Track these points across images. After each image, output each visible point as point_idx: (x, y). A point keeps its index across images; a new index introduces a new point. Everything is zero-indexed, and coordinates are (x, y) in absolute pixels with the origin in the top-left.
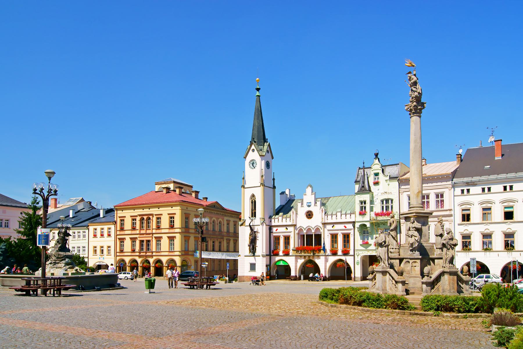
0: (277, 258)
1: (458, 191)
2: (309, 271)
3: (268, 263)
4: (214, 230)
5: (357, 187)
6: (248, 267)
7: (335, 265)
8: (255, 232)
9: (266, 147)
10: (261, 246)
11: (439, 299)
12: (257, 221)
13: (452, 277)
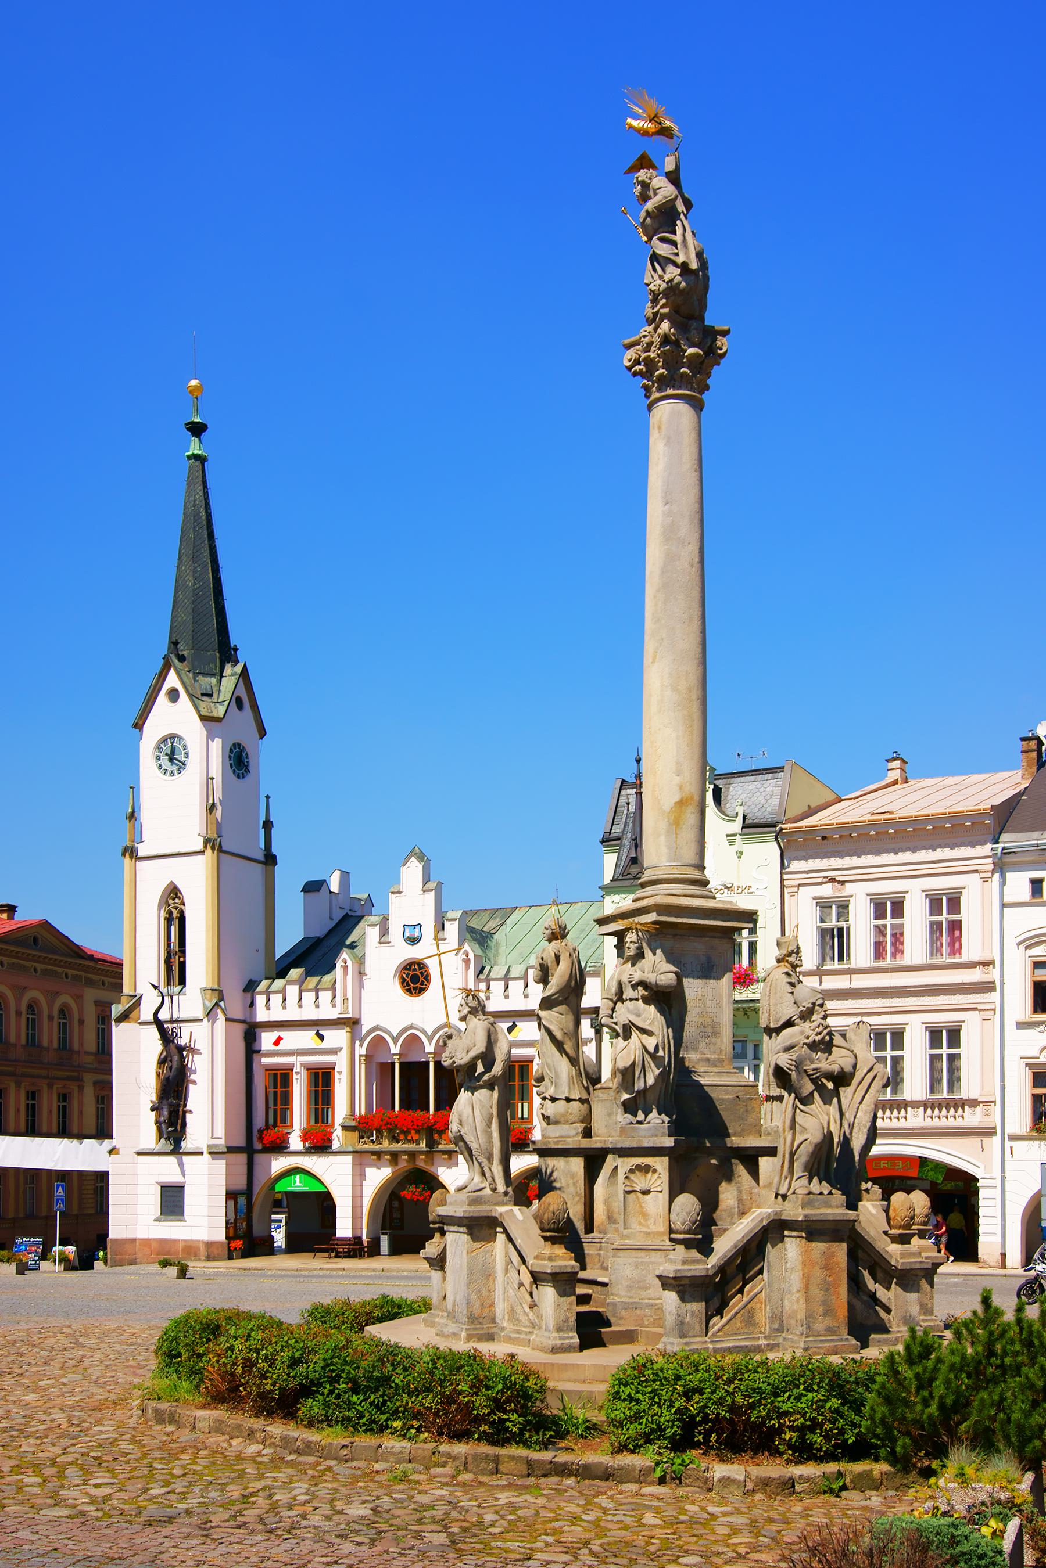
0: (279, 1164)
1: (1018, 883)
3: (241, 1183)
4: (33, 1041)
5: (610, 862)
6: (153, 1201)
8: (181, 1049)
9: (228, 683)
11: (695, 1380)
12: (191, 1002)
13: (819, 1247)
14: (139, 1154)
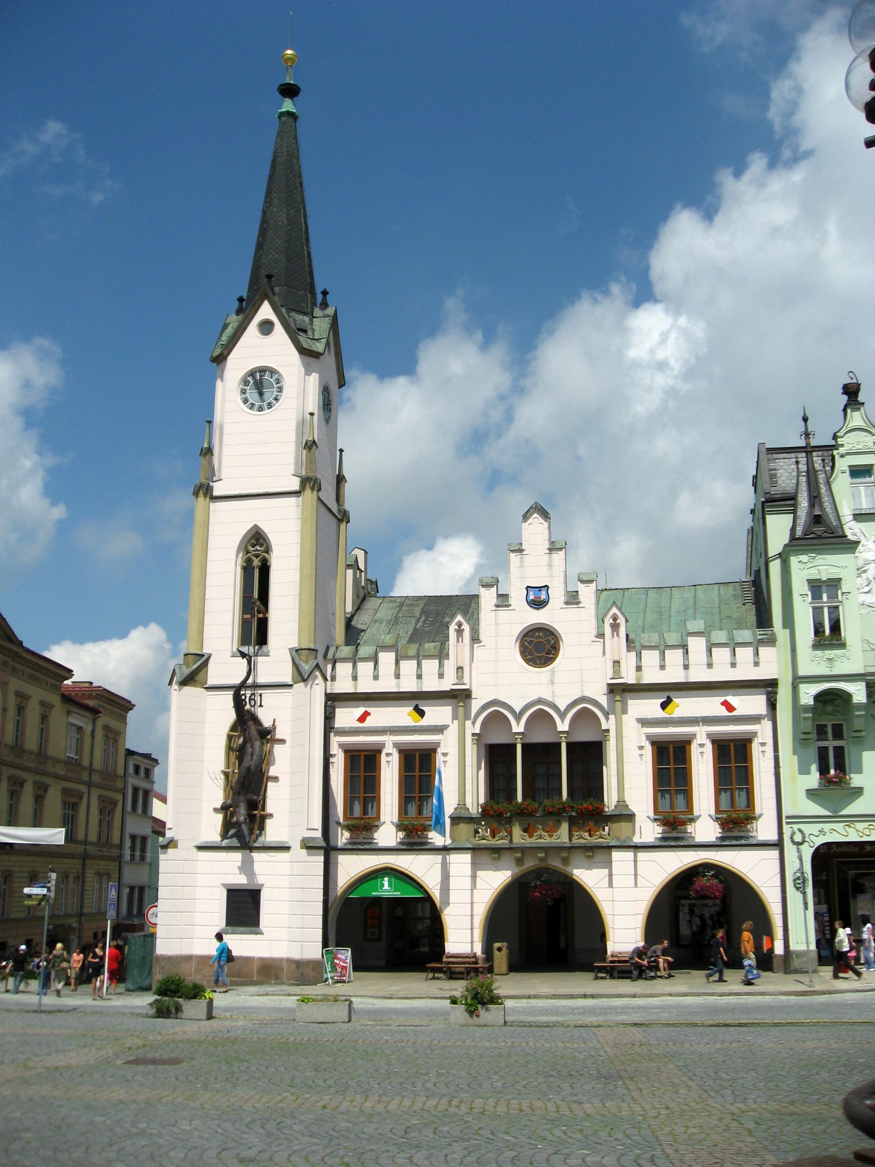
2: (547, 927)
7: (679, 891)
10: (293, 801)
14: (200, 848)
